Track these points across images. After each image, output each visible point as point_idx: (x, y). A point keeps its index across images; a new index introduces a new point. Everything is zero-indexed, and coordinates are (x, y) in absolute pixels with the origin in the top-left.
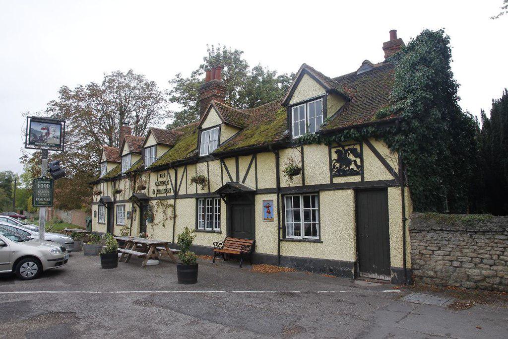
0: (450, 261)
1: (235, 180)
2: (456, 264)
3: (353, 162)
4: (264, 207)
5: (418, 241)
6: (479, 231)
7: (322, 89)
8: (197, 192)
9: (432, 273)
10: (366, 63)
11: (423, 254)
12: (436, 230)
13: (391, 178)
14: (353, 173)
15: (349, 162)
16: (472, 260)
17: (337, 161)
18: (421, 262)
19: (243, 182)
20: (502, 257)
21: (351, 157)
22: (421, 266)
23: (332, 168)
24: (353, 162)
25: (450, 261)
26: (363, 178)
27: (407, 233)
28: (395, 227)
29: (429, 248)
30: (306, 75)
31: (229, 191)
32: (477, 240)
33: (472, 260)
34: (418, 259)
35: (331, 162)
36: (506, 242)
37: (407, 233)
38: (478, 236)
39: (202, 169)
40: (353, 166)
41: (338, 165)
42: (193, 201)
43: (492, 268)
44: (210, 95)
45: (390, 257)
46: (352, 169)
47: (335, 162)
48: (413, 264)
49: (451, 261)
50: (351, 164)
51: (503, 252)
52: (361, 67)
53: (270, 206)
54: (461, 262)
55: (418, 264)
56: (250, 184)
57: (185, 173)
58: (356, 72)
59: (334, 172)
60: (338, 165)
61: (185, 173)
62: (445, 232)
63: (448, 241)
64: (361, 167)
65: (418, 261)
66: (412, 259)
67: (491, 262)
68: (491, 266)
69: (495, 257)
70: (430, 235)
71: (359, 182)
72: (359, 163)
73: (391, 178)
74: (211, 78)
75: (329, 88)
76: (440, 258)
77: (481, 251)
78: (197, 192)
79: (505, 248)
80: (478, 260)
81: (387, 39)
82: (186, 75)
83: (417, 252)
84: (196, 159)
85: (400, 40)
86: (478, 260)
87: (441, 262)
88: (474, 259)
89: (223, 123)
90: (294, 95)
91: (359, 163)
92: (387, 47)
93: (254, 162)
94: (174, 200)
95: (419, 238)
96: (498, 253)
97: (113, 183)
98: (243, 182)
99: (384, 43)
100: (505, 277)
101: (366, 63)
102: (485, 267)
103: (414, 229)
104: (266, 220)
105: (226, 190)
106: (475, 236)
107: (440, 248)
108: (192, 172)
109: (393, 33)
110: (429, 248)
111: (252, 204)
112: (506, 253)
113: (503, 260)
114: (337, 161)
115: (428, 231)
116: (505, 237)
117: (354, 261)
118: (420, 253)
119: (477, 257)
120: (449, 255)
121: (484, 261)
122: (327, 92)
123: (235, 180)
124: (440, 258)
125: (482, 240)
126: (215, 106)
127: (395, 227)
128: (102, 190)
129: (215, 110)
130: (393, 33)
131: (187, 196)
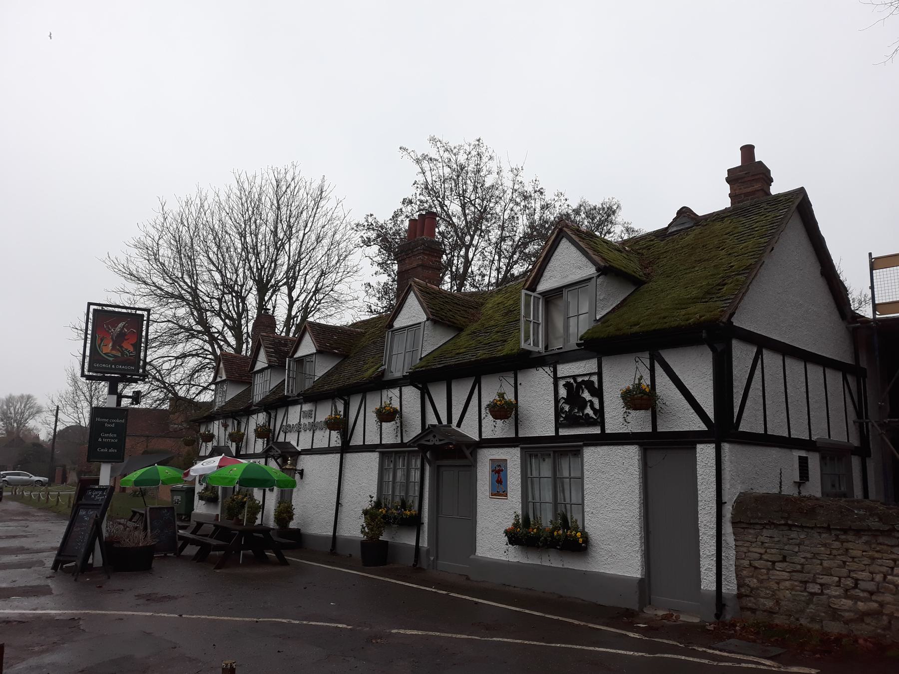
0: (801, 582)
1: (445, 422)
2: (815, 588)
3: (589, 404)
4: (493, 471)
5: (748, 544)
6: (850, 529)
7: (590, 264)
8: (285, 440)
9: (769, 604)
10: (684, 212)
11: (756, 568)
12: (777, 526)
13: (703, 427)
14: (588, 422)
15: (583, 404)
16: (840, 581)
17: (567, 401)
18: (754, 582)
19: (459, 425)
20: (889, 577)
21: (586, 395)
22: (752, 589)
23: (558, 412)
24: (589, 404)
25: (801, 582)
26: (603, 429)
27: (728, 529)
28: (707, 518)
29: (765, 557)
30: (564, 241)
31: (433, 441)
32: (850, 545)
33: (840, 581)
34: (748, 577)
35: (557, 401)
36: (895, 550)
37: (728, 529)
38: (850, 537)
39: (391, 396)
40: (588, 411)
41: (567, 408)
42: (374, 457)
43: (874, 598)
44: (415, 265)
45: (700, 572)
46: (588, 414)
47: (563, 403)
48: (739, 586)
49: (806, 582)
50: (585, 407)
51: (892, 568)
52: (675, 220)
53: (502, 470)
54: (821, 585)
55: (748, 586)
56: (470, 430)
57: (363, 405)
58: (666, 229)
59: (562, 419)
60: (567, 408)
61: (363, 405)
62: (793, 529)
63: (799, 545)
64: (600, 412)
65: (747, 581)
66: (737, 576)
67: (871, 586)
68: (872, 593)
69: (879, 578)
70: (766, 533)
71: (513, 438)
72: (597, 406)
73: (703, 427)
74: (418, 233)
75: (602, 264)
76: (785, 575)
77: (854, 566)
78: (285, 440)
79: (895, 560)
80: (850, 583)
81: (737, 162)
82: (384, 217)
83: (746, 563)
84: (381, 383)
85: (760, 163)
86: (850, 583)
87: (787, 584)
88: (843, 580)
89: (428, 320)
90: (545, 274)
91: (597, 406)
92: (733, 177)
93: (426, 397)
94: (339, 455)
95: (750, 538)
96: (884, 569)
97: (236, 422)
98: (459, 425)
99: (729, 171)
100: (895, 615)
101: (684, 212)
102: (861, 594)
103: (740, 522)
104: (495, 495)
105: (427, 439)
106: (843, 537)
107: (784, 559)
108: (373, 403)
109: (748, 151)
110: (765, 557)
111: (472, 466)
112: (897, 570)
113: (893, 583)
114: (567, 401)
115: (764, 526)
116: (893, 542)
117: (639, 576)
118: (750, 565)
119: (849, 577)
120: (801, 572)
121: (862, 585)
122: (598, 270)
123: (445, 422)
124: (785, 575)
125: (857, 546)
126: (416, 289)
127: (707, 518)
128: (216, 433)
129: (309, 333)
130: (748, 151)
131: (366, 448)
